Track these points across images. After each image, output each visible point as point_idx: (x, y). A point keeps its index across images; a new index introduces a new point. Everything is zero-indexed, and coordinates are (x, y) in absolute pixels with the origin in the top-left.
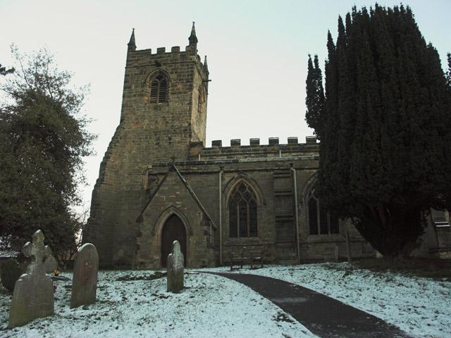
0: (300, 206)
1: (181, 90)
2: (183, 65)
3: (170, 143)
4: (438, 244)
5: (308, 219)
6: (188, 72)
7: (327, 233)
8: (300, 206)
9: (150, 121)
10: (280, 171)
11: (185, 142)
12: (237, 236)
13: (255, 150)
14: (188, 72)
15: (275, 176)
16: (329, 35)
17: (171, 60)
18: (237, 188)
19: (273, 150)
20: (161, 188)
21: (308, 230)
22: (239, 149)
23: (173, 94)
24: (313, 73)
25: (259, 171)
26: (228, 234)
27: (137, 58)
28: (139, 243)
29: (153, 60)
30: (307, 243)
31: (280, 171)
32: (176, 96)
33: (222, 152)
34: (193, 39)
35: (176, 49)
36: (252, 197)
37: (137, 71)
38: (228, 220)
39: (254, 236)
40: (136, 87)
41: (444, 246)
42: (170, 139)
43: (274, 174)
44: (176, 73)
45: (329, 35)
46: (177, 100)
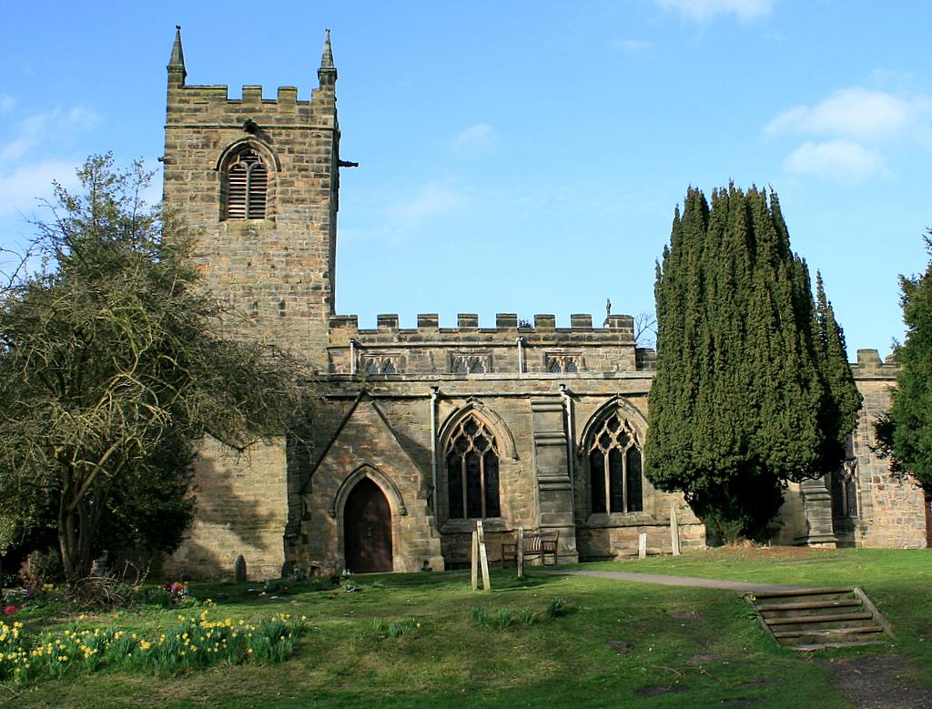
0: (577, 463)
1: (304, 195)
2: (307, 136)
3: (283, 314)
4: (809, 528)
5: (590, 486)
6: (318, 152)
7: (622, 511)
8: (577, 463)
9: (234, 262)
10: (543, 399)
11: (316, 315)
12: (462, 517)
13: (469, 339)
14: (318, 152)
15: (535, 407)
16: (677, 210)
17: (278, 120)
18: (462, 427)
19: (505, 339)
20: (343, 432)
21: (590, 506)
22: (437, 335)
23: (285, 201)
24: (658, 268)
25: (506, 396)
26: (447, 512)
27: (192, 106)
28: (306, 532)
29: (235, 116)
30: (589, 528)
31: (543, 399)
32: (291, 207)
33: (400, 339)
34: (328, 76)
35: (287, 92)
36: (491, 445)
37: (196, 139)
38: (446, 486)
39: (495, 516)
40: (195, 177)
41: (817, 533)
42: (282, 305)
43: (533, 404)
44: (291, 151)
45: (677, 210)
46: (295, 216)
